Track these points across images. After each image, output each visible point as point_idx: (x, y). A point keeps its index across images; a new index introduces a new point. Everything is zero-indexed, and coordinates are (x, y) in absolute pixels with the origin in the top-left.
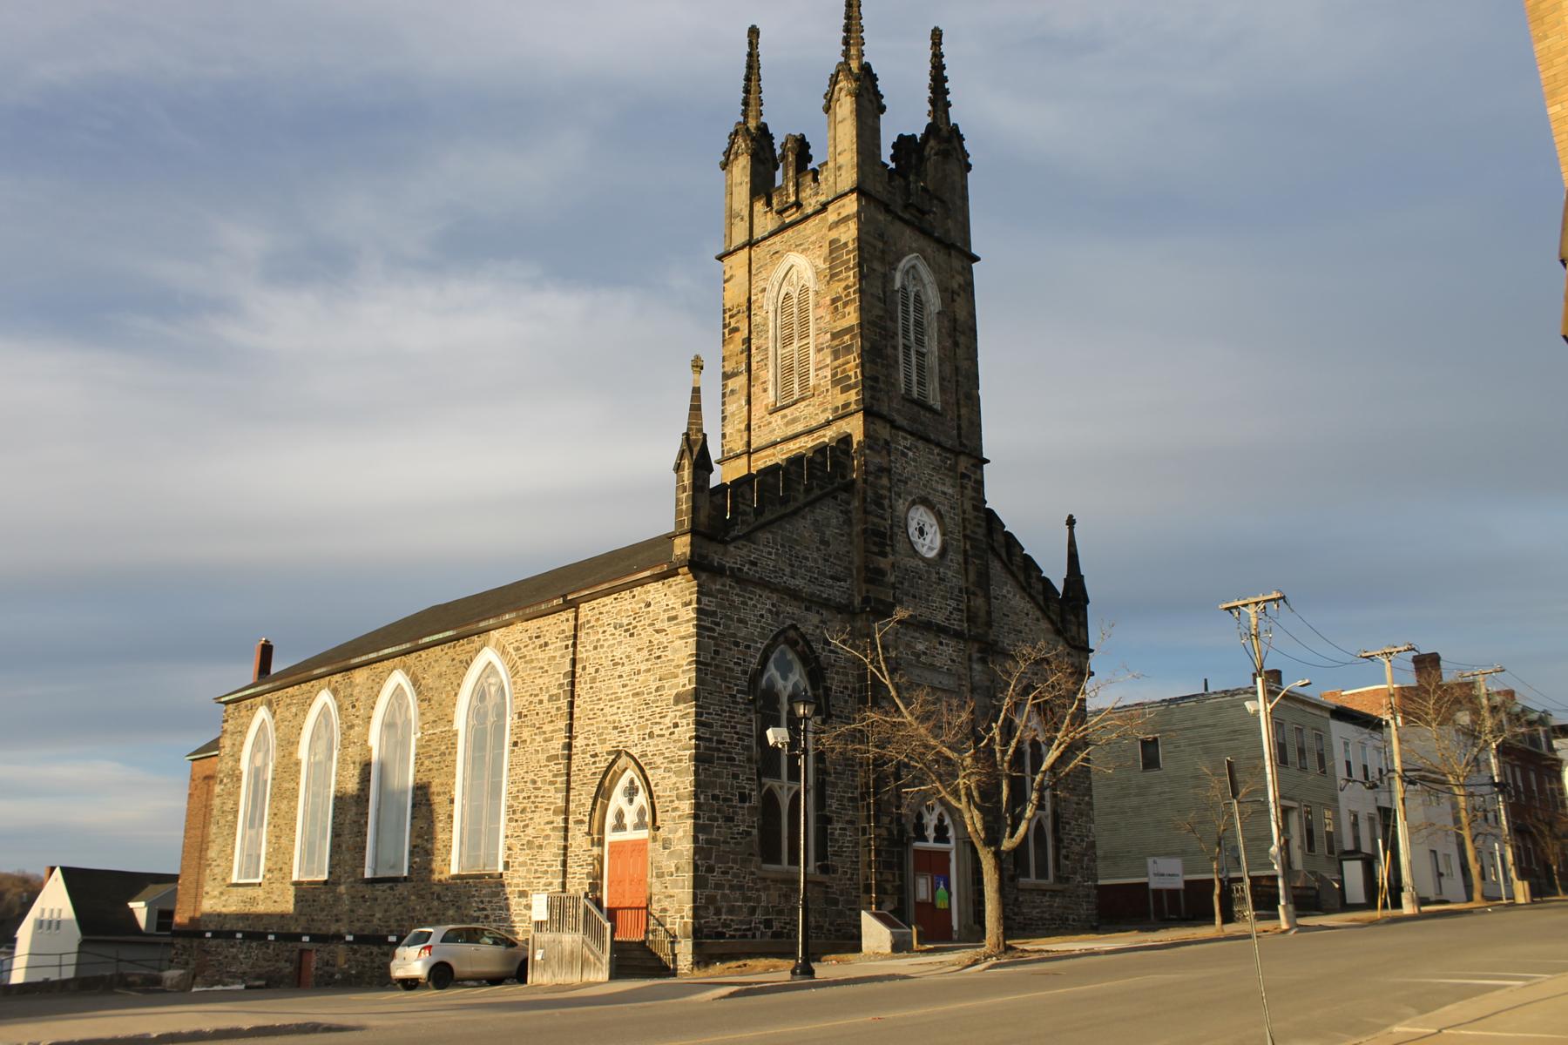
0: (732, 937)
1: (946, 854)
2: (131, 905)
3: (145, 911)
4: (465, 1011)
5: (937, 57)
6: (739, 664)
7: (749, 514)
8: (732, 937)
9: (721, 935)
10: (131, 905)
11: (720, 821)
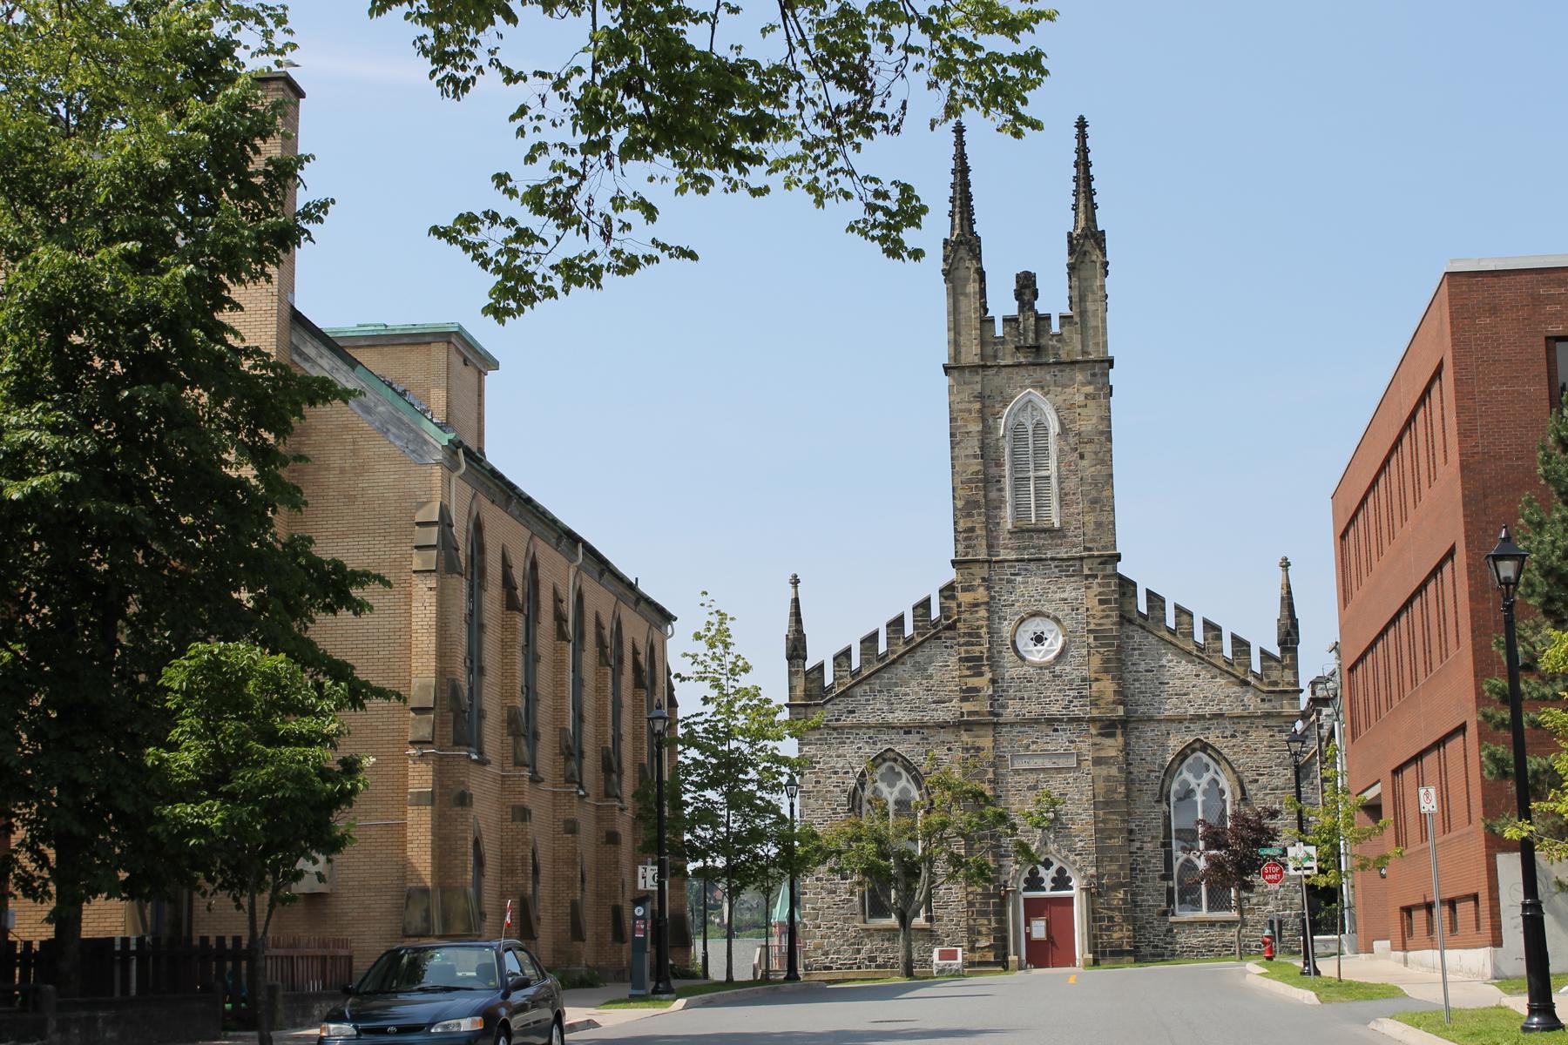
0: (838, 969)
1: (1069, 900)
2: (127, 875)
3: (54, 856)
4: (622, 1005)
5: (1083, 151)
6: (839, 786)
7: (846, 677)
8: (838, 969)
9: (831, 968)
10: (127, 875)
11: (824, 894)
